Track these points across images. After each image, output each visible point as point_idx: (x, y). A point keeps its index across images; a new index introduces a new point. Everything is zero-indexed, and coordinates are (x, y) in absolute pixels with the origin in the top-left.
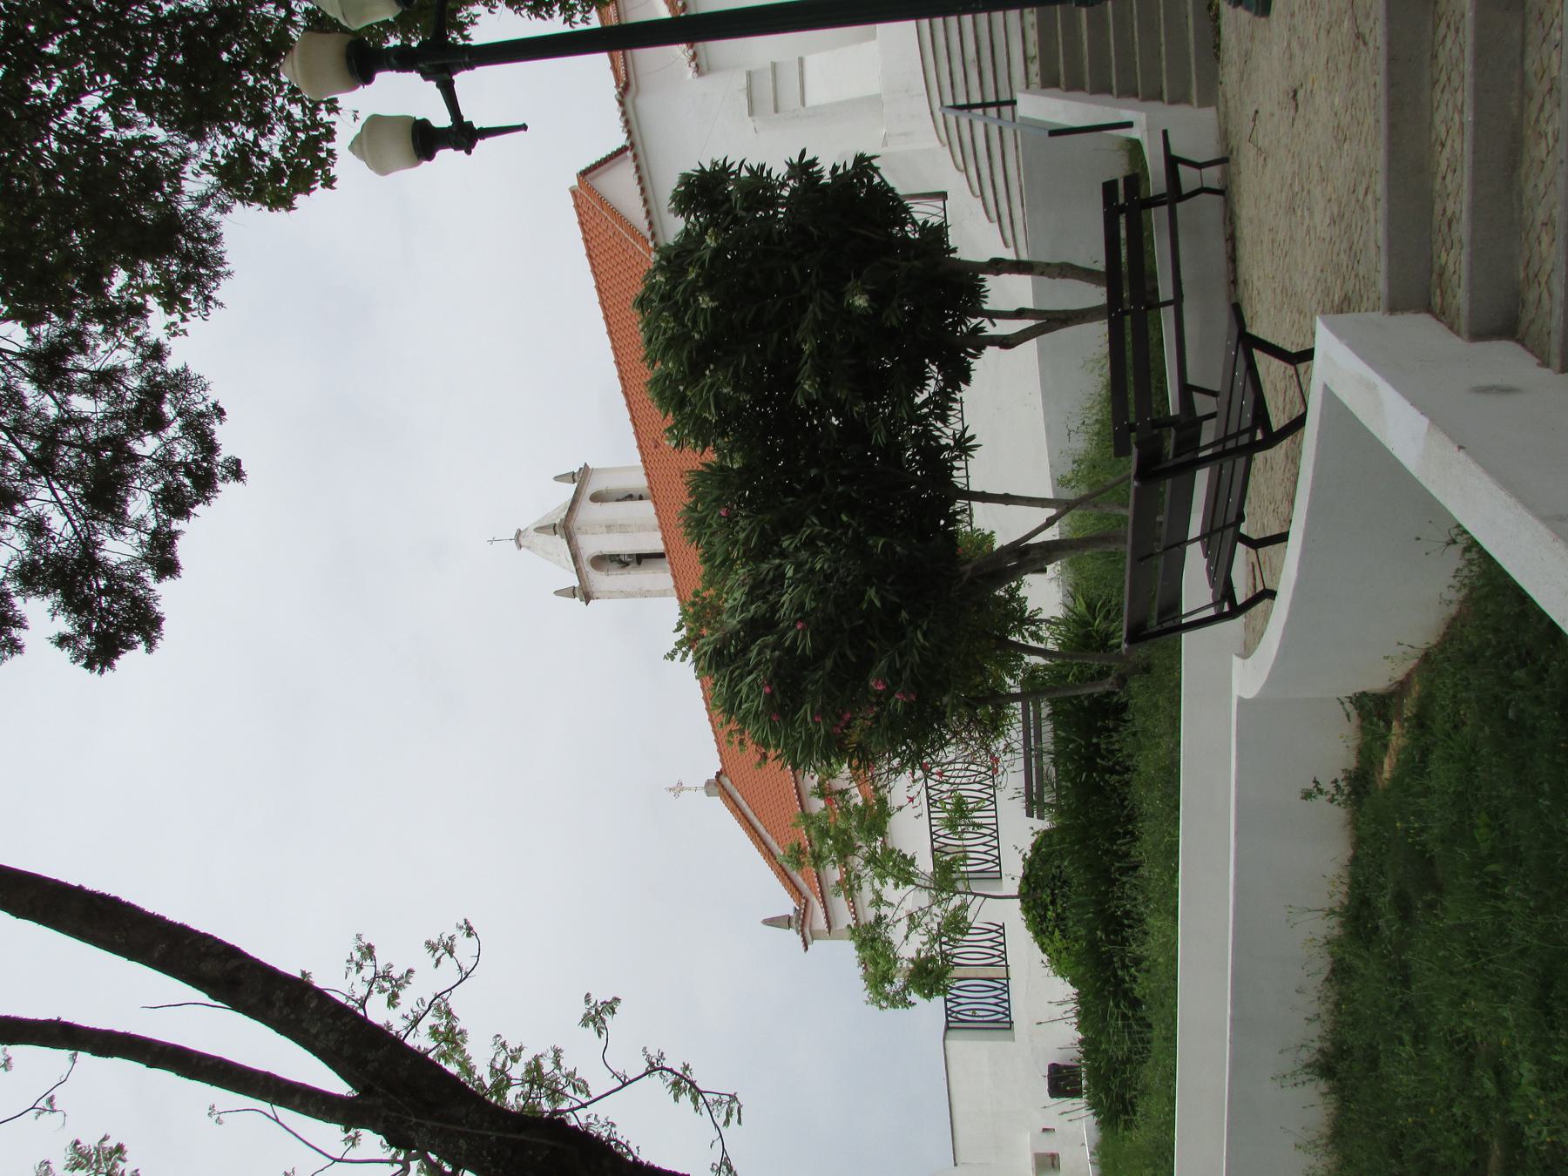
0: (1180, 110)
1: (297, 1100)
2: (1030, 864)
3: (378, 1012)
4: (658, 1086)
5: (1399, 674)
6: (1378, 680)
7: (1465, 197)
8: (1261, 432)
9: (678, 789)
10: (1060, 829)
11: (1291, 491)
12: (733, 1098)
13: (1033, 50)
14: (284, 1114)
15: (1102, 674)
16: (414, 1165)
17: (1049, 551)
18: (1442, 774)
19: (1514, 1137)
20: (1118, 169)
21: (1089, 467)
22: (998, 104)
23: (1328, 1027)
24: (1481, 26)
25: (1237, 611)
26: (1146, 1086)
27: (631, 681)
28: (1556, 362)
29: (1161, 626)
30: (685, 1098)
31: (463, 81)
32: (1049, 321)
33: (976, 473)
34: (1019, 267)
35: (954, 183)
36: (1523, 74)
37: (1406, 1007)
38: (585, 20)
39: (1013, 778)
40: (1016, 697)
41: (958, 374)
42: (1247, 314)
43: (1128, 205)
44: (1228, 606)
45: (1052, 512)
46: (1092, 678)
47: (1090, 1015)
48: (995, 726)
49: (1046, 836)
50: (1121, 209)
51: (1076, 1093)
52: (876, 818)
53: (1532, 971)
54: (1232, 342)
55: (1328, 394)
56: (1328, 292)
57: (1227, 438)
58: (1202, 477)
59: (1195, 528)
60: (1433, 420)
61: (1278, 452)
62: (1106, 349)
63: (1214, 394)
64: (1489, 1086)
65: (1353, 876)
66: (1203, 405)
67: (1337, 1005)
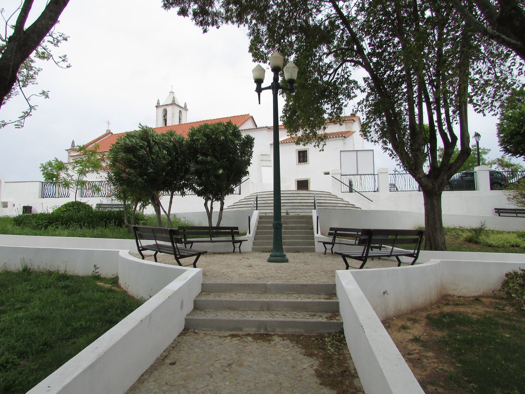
0: (252, 244)
1: (23, 14)
2: (84, 204)
3: (47, 38)
4: (26, 108)
5: (122, 286)
6: (121, 282)
7: (224, 299)
8: (178, 257)
9: (108, 123)
10: (92, 211)
11: (167, 262)
12: (23, 126)
13: (267, 214)
14: (19, 11)
15: (129, 222)
16: (5, 43)
17: (158, 211)
18: (97, 295)
19: (4, 312)
20: (240, 230)
21: (178, 221)
22: (257, 207)
23: (36, 270)
24: (259, 302)
25: (140, 251)
26: (24, 229)
27: (134, 114)
28: (187, 317)
29: (137, 234)
30: (23, 114)
31: (270, 91)
32: (210, 215)
33: (177, 197)
34: (222, 209)
35: (242, 197)
36: (247, 311)
37: (40, 288)
38: (281, 120)
39: (105, 201)
40: (125, 203)
41: (199, 193)
42: (205, 255)
43: (233, 232)
44: (141, 249)
45: (167, 212)
46: (128, 220)
47: (43, 216)
48: (119, 197)
49: (91, 208)
50: (232, 231)
51: (23, 213)
52: (96, 167)
53: (46, 315)
54: (199, 251)
55: (186, 270)
56: (208, 272)
57: (178, 250)
58: (170, 244)
59: (159, 242)
60: (176, 292)
61: (175, 261)
62: (203, 226)
63: (191, 248)
64: (17, 306)
65: (74, 276)
66: (188, 246)
67: (42, 272)
